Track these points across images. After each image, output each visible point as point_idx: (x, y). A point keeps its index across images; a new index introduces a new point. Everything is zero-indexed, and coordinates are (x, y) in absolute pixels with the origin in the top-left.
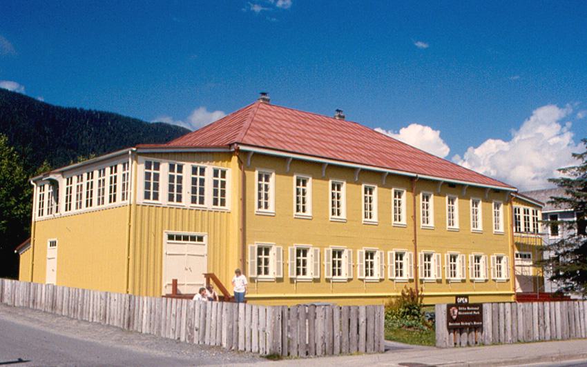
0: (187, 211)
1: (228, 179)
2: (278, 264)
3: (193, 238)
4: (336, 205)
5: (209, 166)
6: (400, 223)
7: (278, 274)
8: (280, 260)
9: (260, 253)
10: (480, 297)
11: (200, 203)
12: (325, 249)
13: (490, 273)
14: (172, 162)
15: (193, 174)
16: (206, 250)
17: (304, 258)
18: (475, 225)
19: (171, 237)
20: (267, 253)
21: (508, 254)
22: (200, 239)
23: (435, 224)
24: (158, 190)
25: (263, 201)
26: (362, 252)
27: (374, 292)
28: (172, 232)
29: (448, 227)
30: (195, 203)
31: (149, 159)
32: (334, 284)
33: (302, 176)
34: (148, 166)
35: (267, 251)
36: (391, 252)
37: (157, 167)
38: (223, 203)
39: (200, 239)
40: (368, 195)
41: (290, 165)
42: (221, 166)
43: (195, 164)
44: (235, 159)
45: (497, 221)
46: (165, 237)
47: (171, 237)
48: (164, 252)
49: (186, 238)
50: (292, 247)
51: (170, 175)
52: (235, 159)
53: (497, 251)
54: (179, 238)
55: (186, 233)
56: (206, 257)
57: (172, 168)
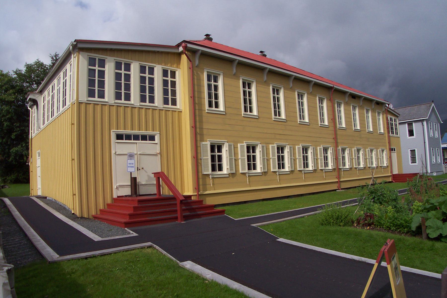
0: (136, 110)
1: (178, 79)
2: (231, 160)
3: (144, 138)
4: (248, 102)
5: (157, 66)
6: (279, 117)
7: (231, 170)
8: (232, 156)
9: (212, 150)
10: (353, 182)
11: (125, 100)
12: (270, 146)
13: (317, 163)
14: (119, 59)
15: (164, 77)
16: (158, 147)
17: (254, 154)
18: (302, 117)
19: (119, 137)
20: (220, 150)
21: (386, 149)
22: (152, 138)
23: (328, 124)
24: (153, 93)
25: (213, 102)
26: (300, 148)
27: (348, 178)
28: (121, 131)
29: (299, 120)
30: (168, 104)
31: (93, 55)
32: (306, 174)
33: (214, 71)
34: (92, 62)
35: (220, 149)
36: (299, 146)
37: (102, 63)
38: (174, 102)
39: (152, 138)
40: (247, 89)
41: (236, 66)
42: (171, 67)
43: (166, 67)
44: (184, 58)
45: (322, 115)
46: (113, 136)
47: (119, 137)
48: (113, 152)
49: (136, 137)
50: (299, 146)
51: (116, 73)
52: (184, 58)
53: (303, 141)
54: (128, 137)
55: (128, 131)
56: (159, 156)
57: (118, 66)
